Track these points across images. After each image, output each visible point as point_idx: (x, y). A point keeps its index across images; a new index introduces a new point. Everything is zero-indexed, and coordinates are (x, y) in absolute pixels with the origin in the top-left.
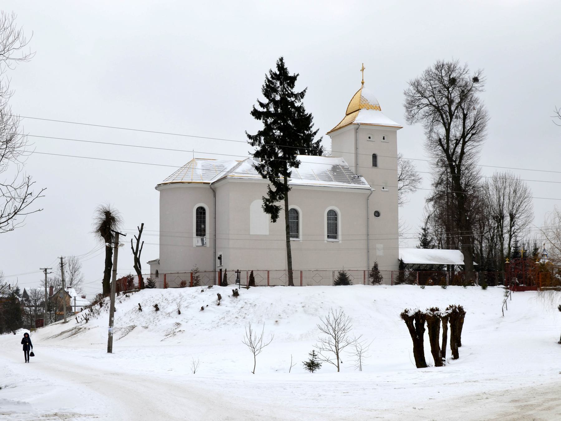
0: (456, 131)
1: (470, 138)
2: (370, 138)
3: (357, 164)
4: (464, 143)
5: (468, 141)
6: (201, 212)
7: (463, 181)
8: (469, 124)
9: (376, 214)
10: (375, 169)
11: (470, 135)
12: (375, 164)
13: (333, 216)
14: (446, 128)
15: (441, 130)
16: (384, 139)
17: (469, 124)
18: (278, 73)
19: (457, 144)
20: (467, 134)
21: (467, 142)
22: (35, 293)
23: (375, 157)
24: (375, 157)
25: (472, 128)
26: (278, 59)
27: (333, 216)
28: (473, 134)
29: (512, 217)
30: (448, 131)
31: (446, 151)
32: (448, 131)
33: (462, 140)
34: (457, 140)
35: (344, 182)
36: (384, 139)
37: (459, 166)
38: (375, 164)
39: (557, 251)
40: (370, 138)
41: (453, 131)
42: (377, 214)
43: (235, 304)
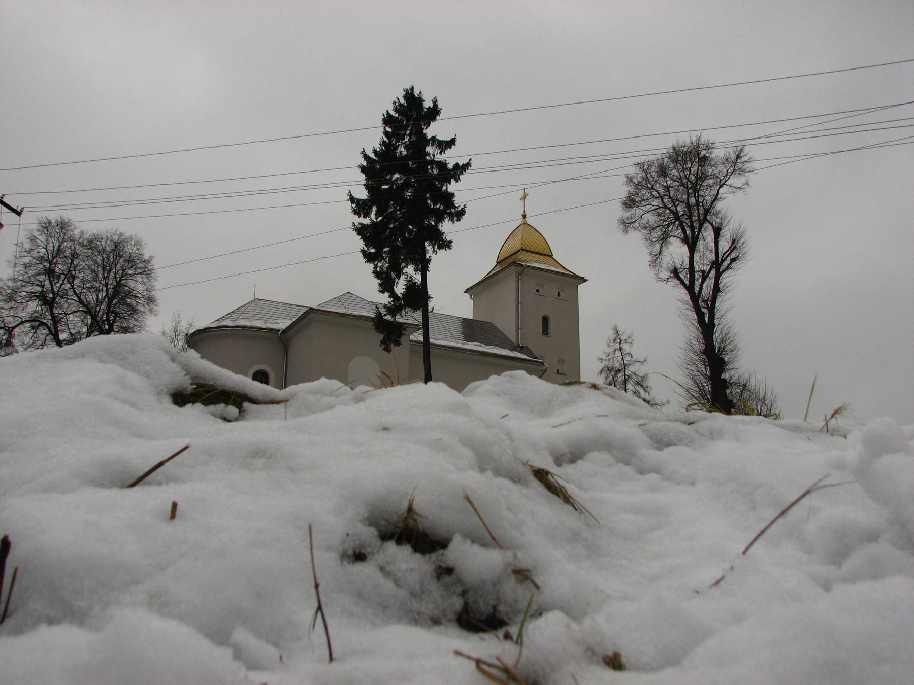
2: (538, 291)
3: (518, 329)
4: (718, 275)
5: (727, 268)
7: (717, 336)
8: (724, 245)
11: (726, 264)
12: (546, 331)
15: (677, 252)
16: (559, 295)
17: (724, 245)
18: (392, 345)
20: (723, 261)
21: (723, 271)
23: (545, 320)
24: (545, 320)
25: (733, 248)
26: (388, 100)
28: (733, 260)
31: (690, 288)
34: (703, 272)
35: (504, 347)
36: (559, 295)
37: (712, 310)
38: (546, 331)
40: (538, 291)
43: (529, 515)
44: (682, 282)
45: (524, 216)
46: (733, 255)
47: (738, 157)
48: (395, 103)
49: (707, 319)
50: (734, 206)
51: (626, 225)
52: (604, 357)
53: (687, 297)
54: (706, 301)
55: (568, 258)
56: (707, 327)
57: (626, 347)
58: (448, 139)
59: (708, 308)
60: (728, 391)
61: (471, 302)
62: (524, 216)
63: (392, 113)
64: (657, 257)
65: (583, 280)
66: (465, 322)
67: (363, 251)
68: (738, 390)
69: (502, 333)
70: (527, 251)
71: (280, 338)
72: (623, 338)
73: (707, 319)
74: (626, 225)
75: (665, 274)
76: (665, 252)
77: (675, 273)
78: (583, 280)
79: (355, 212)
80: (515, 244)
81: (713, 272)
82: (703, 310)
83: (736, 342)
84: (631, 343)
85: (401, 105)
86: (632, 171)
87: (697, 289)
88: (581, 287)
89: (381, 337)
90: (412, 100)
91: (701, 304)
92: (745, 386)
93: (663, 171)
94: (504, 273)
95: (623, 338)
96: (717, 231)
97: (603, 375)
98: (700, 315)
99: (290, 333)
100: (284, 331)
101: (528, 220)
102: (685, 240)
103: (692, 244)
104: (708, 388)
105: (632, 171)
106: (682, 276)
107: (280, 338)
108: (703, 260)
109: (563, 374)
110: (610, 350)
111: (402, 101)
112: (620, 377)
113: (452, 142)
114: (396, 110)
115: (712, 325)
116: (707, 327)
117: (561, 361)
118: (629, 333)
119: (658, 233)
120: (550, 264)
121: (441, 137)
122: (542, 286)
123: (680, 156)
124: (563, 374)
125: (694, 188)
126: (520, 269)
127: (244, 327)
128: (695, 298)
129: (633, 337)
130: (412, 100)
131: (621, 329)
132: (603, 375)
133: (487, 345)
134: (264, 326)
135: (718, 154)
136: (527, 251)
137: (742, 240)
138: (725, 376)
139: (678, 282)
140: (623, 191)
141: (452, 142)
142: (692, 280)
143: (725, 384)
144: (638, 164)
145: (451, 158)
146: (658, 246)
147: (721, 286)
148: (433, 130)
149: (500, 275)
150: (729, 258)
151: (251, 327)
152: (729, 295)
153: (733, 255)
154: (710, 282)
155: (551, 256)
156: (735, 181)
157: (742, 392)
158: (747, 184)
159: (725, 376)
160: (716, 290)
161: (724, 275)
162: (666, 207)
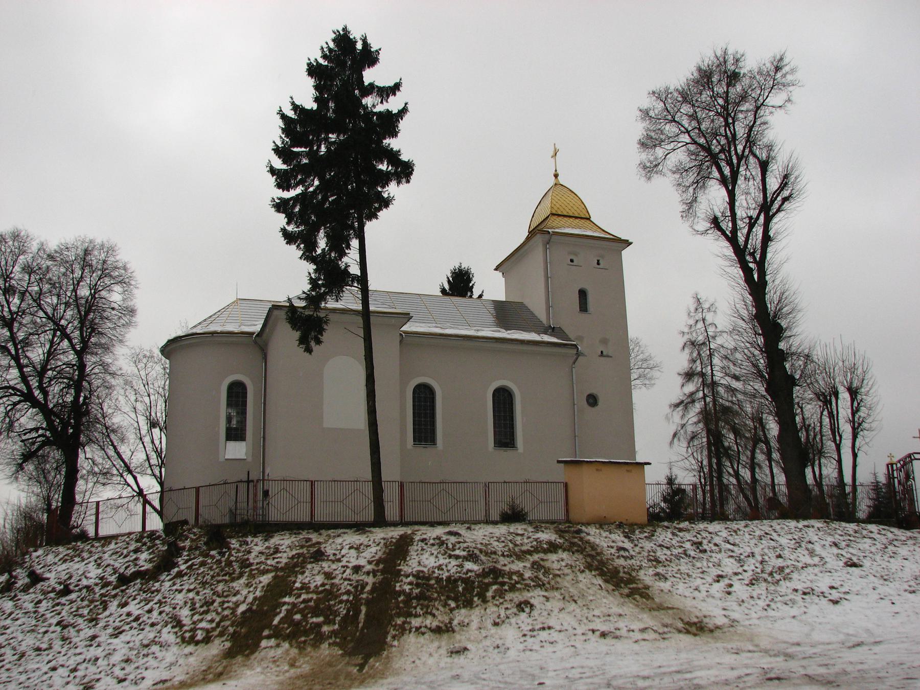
0: (748, 201)
1: (780, 206)
2: (572, 261)
3: (548, 307)
5: (779, 210)
6: (237, 393)
7: (772, 296)
8: (773, 184)
9: (591, 401)
10: (583, 316)
11: (776, 206)
12: (583, 307)
13: (503, 401)
14: (727, 188)
15: (715, 196)
16: (598, 264)
17: (773, 184)
19: (751, 226)
20: (772, 202)
21: (774, 215)
22: (877, 486)
23: (583, 294)
24: (583, 294)
25: (783, 186)
26: (314, 45)
27: (503, 401)
28: (785, 200)
29: (853, 392)
30: (732, 195)
31: (732, 239)
32: (732, 195)
33: (762, 217)
34: (750, 218)
36: (598, 264)
37: (761, 264)
38: (583, 307)
39: (8, 605)
41: (740, 200)
42: (592, 400)
44: (723, 233)
45: (556, 176)
46: (786, 193)
47: (777, 69)
48: (322, 48)
49: (756, 276)
50: (786, 130)
51: (651, 169)
52: (686, 330)
53: (729, 251)
54: (752, 254)
55: (607, 218)
56: (757, 286)
57: (709, 317)
58: (391, 84)
59: (755, 261)
60: (787, 366)
61: (502, 280)
62: (556, 176)
63: (321, 61)
64: (691, 205)
65: (628, 243)
66: (498, 305)
67: (284, 231)
68: (801, 363)
69: (532, 313)
70: (559, 215)
71: (255, 342)
72: (706, 306)
73: (756, 276)
74: (651, 169)
75: (704, 225)
76: (702, 198)
77: (715, 222)
78: (628, 243)
79: (279, 186)
80: (545, 211)
81: (762, 217)
82: (751, 265)
83: (796, 301)
84: (715, 311)
85: (330, 50)
86: (647, 102)
87: (741, 239)
88: (626, 253)
89: (297, 335)
90: (343, 40)
91: (748, 258)
92: (807, 356)
93: (685, 97)
94: (530, 243)
95: (706, 306)
96: (764, 166)
97: (687, 351)
98: (747, 272)
99: (264, 336)
100: (260, 334)
101: (561, 180)
102: (723, 181)
103: (729, 184)
104: (762, 363)
105: (647, 102)
106: (723, 226)
107: (255, 342)
108: (747, 205)
109: (608, 356)
110: (692, 322)
111: (332, 45)
112: (705, 353)
113: (396, 87)
114: (324, 57)
115: (763, 283)
116: (757, 286)
117: (605, 341)
118: (711, 300)
119: (691, 177)
120: (586, 228)
121: (380, 83)
122: (576, 255)
123: (705, 77)
124: (608, 356)
125: (728, 114)
126: (547, 236)
127: (213, 333)
128: (740, 252)
129: (717, 304)
130: (343, 40)
131: (702, 296)
132: (687, 351)
133: (507, 329)
134: (236, 330)
135: (749, 65)
136: (559, 215)
137: (796, 174)
138: (782, 345)
139: (719, 233)
140: (639, 129)
141: (396, 87)
142: (735, 230)
143: (782, 356)
144: (654, 93)
145: (393, 104)
146: (691, 190)
147: (771, 234)
148: (370, 76)
149: (526, 247)
150: (779, 198)
151: (222, 333)
152: (784, 242)
153: (786, 193)
154: (758, 230)
155: (589, 219)
156: (775, 99)
157: (805, 364)
158: (789, 100)
159: (782, 345)
160: (767, 239)
161: (775, 220)
162: (695, 143)
